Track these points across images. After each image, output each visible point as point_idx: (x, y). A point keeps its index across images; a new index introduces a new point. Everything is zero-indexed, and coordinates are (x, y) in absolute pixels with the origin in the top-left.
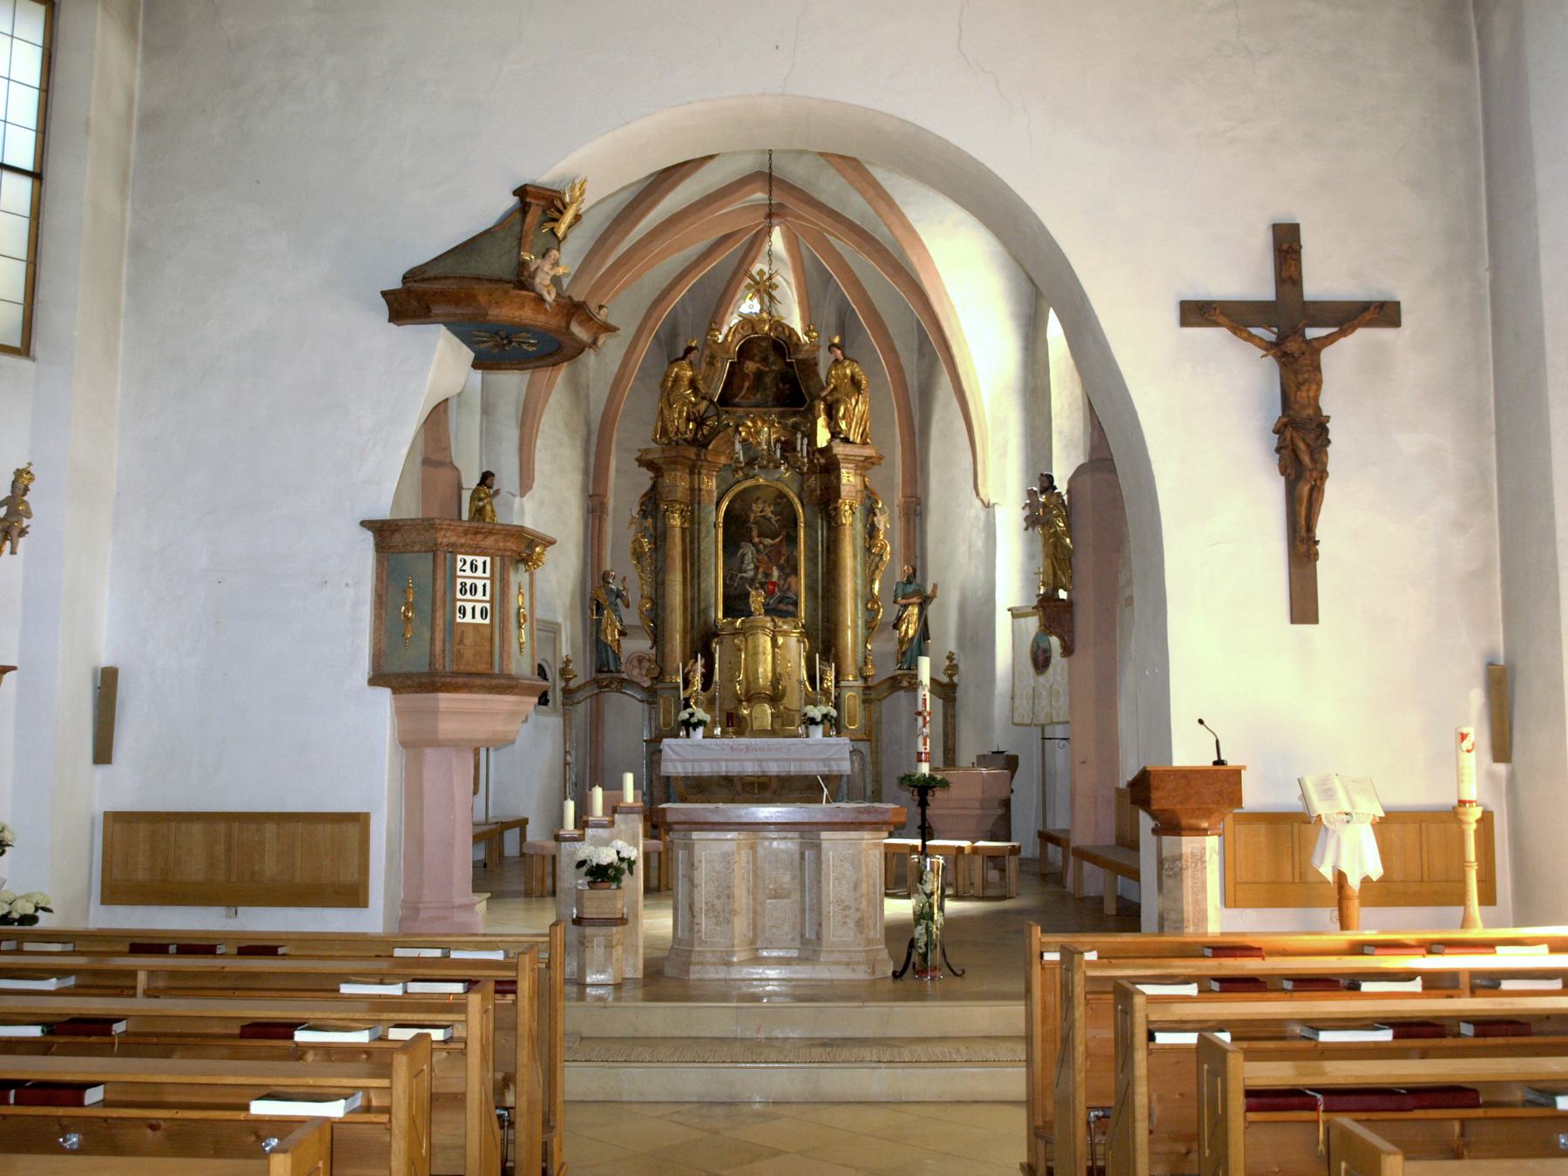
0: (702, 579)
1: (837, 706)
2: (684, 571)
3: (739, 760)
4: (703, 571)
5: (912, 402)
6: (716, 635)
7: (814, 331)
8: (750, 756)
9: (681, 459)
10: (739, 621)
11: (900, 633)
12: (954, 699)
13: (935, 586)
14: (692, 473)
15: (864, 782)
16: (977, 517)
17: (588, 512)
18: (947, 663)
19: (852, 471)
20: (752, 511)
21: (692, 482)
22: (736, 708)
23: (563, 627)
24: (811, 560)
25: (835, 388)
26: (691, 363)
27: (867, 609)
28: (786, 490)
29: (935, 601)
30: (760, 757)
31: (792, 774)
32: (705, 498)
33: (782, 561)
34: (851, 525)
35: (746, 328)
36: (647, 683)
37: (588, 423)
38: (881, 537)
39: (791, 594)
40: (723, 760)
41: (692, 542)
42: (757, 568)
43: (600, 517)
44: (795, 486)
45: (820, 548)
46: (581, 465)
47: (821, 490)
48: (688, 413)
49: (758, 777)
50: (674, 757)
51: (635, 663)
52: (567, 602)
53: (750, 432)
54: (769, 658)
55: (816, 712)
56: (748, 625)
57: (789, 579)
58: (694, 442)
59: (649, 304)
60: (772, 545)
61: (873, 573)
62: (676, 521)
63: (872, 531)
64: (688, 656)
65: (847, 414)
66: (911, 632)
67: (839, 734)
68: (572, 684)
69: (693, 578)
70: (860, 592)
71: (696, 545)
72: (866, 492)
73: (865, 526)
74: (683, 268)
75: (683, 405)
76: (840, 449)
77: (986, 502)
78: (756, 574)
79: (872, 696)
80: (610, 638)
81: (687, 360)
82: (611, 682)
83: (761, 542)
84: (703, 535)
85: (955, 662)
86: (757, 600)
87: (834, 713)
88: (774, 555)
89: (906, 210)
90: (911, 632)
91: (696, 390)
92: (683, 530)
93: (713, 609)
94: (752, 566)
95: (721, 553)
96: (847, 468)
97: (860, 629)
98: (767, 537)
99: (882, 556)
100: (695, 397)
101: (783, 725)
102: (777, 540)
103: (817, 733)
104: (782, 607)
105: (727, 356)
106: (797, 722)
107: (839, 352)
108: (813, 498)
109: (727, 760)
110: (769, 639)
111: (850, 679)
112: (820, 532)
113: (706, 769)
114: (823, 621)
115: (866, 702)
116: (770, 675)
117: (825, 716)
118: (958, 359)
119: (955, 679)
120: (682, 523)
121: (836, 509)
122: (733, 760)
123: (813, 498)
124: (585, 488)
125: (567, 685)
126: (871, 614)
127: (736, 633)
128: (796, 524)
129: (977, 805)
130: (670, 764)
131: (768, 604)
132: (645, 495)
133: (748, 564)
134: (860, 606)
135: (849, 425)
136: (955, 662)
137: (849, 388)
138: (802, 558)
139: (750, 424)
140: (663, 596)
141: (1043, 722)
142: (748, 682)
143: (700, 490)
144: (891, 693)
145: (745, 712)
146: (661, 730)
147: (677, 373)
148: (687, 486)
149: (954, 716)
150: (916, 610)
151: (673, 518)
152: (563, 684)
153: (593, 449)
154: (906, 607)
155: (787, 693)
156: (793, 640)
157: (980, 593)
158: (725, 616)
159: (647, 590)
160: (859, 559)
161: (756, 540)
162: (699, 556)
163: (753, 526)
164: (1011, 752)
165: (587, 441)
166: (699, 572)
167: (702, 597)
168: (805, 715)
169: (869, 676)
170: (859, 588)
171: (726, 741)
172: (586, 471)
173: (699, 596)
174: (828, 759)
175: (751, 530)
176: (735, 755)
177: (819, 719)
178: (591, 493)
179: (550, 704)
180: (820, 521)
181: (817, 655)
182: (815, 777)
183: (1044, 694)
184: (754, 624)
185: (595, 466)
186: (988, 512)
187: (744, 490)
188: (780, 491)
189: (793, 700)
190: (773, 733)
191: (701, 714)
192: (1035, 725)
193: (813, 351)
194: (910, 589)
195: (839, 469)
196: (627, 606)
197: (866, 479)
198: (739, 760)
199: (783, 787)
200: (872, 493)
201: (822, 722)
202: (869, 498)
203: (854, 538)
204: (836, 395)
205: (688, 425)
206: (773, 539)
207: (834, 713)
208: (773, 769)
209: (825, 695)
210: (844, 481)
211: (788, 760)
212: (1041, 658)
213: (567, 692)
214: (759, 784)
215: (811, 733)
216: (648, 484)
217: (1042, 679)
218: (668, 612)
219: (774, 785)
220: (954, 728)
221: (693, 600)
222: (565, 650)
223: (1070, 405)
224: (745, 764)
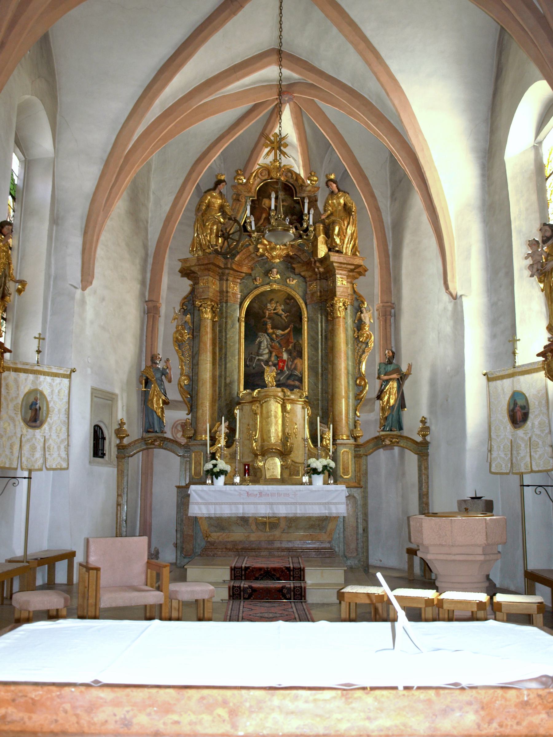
0: (227, 361)
1: (334, 459)
2: (214, 353)
3: (254, 504)
4: (228, 354)
5: (387, 234)
6: (239, 403)
7: (314, 176)
8: (263, 500)
9: (211, 266)
10: (256, 391)
11: (383, 403)
12: (427, 455)
13: (410, 366)
14: (221, 279)
15: (357, 522)
16: (445, 309)
17: (144, 312)
18: (421, 425)
19: (345, 277)
20: (268, 309)
21: (221, 286)
22: (253, 461)
23: (119, 398)
24: (313, 346)
25: (332, 214)
26: (220, 193)
27: (356, 385)
28: (293, 293)
29: (410, 376)
30: (271, 501)
31: (298, 515)
32: (231, 300)
33: (290, 347)
34: (344, 318)
35: (263, 174)
36: (183, 441)
37: (145, 247)
38: (367, 329)
39: (297, 373)
40: (211, 504)
41: (220, 331)
42: (270, 353)
43: (154, 317)
44: (300, 291)
45: (320, 337)
46: (140, 277)
47: (321, 292)
48: (217, 229)
49: (269, 518)
50: (200, 501)
51: (179, 428)
52: (125, 377)
53: (266, 249)
54: (280, 421)
55: (318, 464)
56: (263, 394)
57: (296, 361)
58: (224, 255)
59: (193, 162)
60: (283, 335)
61: (361, 357)
62: (208, 316)
63: (359, 325)
64: (215, 421)
65: (341, 233)
66: (392, 402)
67: (335, 482)
68: (126, 441)
69: (220, 359)
70: (350, 372)
71: (224, 334)
72: (355, 296)
73: (354, 322)
74: (218, 136)
75: (213, 225)
76: (334, 258)
77: (454, 294)
78: (270, 357)
79: (361, 452)
80: (155, 406)
81: (217, 190)
82: (155, 440)
83: (273, 333)
84: (229, 327)
85: (427, 425)
86: (270, 376)
87: (333, 464)
88: (285, 341)
89: (388, 62)
90: (392, 402)
91: (224, 214)
92: (214, 323)
93: (236, 384)
94: (267, 351)
95: (243, 341)
96: (341, 274)
97: (351, 400)
98: (278, 329)
99: (367, 343)
100: (224, 218)
101: (290, 475)
102: (287, 331)
103: (318, 480)
104: (290, 382)
105: (250, 194)
106: (301, 472)
107: (334, 185)
108: (315, 299)
109: (243, 504)
110: (279, 405)
111: (344, 437)
112: (320, 324)
113: (226, 511)
114: (322, 393)
115: (357, 456)
116: (280, 434)
117: (325, 467)
118: (430, 182)
119: (428, 438)
120: (213, 317)
121: (332, 305)
122: (249, 504)
123: (315, 299)
124: (142, 294)
125: (120, 443)
126: (359, 388)
127: (254, 401)
128: (301, 319)
129: (479, 550)
130: (196, 507)
131: (279, 380)
132: (185, 298)
133: (264, 349)
134: (351, 382)
135: (342, 241)
136: (427, 425)
137: (342, 214)
138: (306, 345)
139: (266, 242)
140: (197, 374)
141: (523, 471)
142: (263, 440)
143: (227, 292)
144: (375, 450)
145: (261, 464)
146: (193, 478)
147: (209, 200)
148: (218, 289)
149: (427, 468)
150: (395, 385)
151: (206, 312)
152: (118, 442)
153: (149, 267)
154: (387, 381)
155: (294, 450)
156: (298, 407)
157: (448, 368)
158: (245, 389)
159: (186, 369)
160: (349, 346)
161: (270, 331)
162: (226, 343)
163: (268, 320)
164: (487, 497)
165: (145, 260)
166: (226, 355)
167: (227, 375)
168: (309, 466)
169: (359, 437)
170: (350, 368)
171: (243, 487)
172: (143, 283)
173: (226, 373)
174: (328, 503)
175: (266, 324)
176: (251, 500)
177: (320, 469)
178: (147, 300)
179: (106, 457)
180: (319, 316)
181: (318, 418)
183: (523, 445)
184: (267, 393)
185: (151, 280)
186: (455, 304)
187: (262, 294)
188: (289, 295)
189: (298, 455)
190: (282, 481)
191: (222, 465)
192: (513, 473)
193: (314, 192)
194: (390, 368)
195: (334, 275)
196: (170, 381)
197: (355, 286)
198: (254, 504)
199: (289, 527)
200: (360, 296)
201: (322, 472)
202: (357, 300)
203: (346, 330)
204: (333, 218)
205: (218, 240)
206: (283, 331)
207: (333, 464)
208: (282, 511)
209: (324, 450)
210: (339, 284)
211: (295, 504)
212: (519, 415)
213: (121, 448)
214: (270, 523)
215: (314, 482)
216: (189, 289)
217: (520, 432)
218: (200, 384)
219: (283, 524)
220: (428, 477)
221: (220, 376)
222: (121, 414)
223: (527, 209)
224: (259, 506)
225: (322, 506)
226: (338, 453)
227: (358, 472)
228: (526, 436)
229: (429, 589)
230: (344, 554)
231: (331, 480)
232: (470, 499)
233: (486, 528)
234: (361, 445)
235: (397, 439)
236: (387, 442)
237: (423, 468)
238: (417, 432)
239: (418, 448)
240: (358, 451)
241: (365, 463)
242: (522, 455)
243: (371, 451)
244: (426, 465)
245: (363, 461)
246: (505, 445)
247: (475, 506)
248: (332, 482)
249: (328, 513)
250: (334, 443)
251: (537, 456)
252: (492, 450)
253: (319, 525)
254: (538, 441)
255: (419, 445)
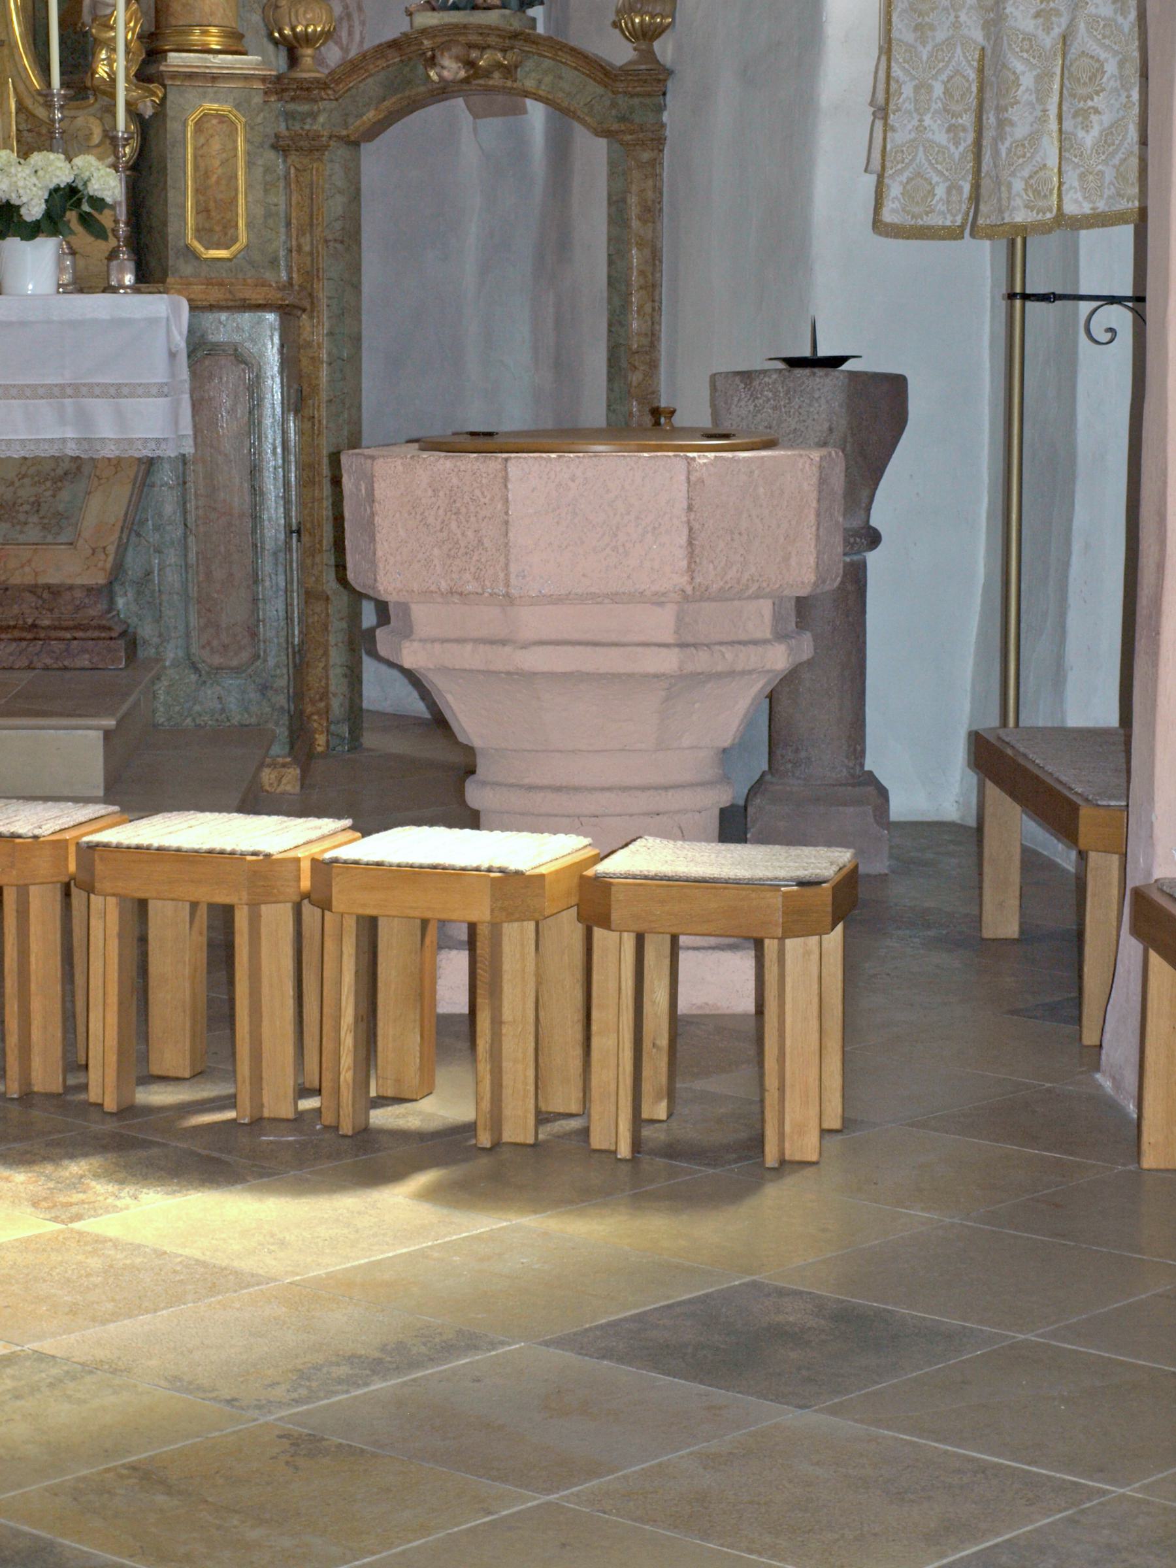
119: (664, 49)
149: (651, 211)
169: (307, 40)
174: (77, 390)
177: (34, 211)
182: (846, 565)
183: (1027, 80)
201: (50, 224)
220: (655, 258)
225: (43, 406)
226: (172, 126)
227: (301, 232)
228: (1048, 29)
229: (202, 809)
230: (188, 655)
231: (122, 271)
232: (781, 365)
233: (690, 508)
234: (323, 85)
235: (504, 50)
236: (450, 68)
237: (634, 211)
238: (613, 17)
239: (614, 105)
240: (303, 117)
241: (339, 180)
242: (1020, 131)
243: (371, 115)
244: (650, 194)
245: (332, 168)
246: (950, 78)
247: (797, 401)
248: (129, 279)
249: (78, 441)
250: (152, 70)
251: (1089, 139)
252: (892, 107)
253: (37, 505)
254: (1103, 55)
255: (621, 86)
